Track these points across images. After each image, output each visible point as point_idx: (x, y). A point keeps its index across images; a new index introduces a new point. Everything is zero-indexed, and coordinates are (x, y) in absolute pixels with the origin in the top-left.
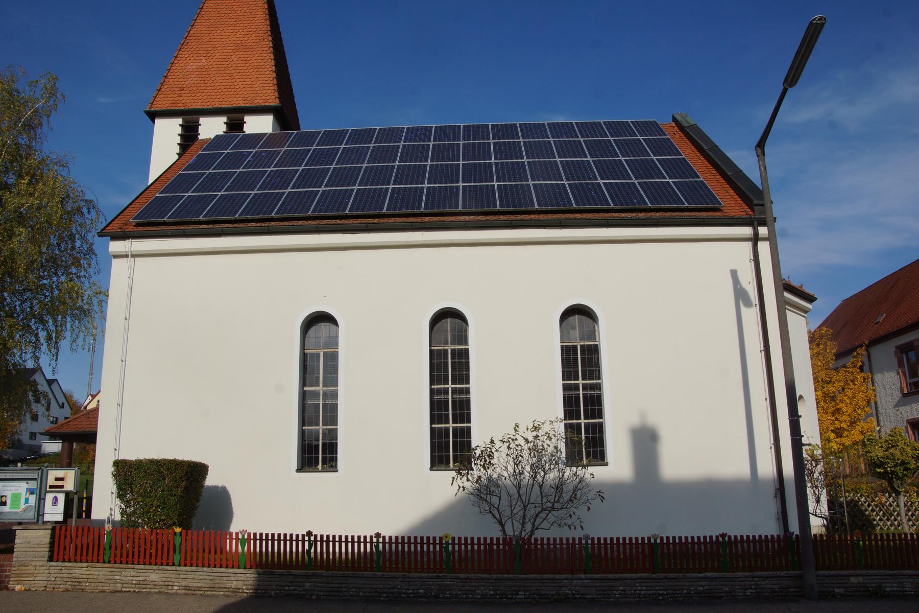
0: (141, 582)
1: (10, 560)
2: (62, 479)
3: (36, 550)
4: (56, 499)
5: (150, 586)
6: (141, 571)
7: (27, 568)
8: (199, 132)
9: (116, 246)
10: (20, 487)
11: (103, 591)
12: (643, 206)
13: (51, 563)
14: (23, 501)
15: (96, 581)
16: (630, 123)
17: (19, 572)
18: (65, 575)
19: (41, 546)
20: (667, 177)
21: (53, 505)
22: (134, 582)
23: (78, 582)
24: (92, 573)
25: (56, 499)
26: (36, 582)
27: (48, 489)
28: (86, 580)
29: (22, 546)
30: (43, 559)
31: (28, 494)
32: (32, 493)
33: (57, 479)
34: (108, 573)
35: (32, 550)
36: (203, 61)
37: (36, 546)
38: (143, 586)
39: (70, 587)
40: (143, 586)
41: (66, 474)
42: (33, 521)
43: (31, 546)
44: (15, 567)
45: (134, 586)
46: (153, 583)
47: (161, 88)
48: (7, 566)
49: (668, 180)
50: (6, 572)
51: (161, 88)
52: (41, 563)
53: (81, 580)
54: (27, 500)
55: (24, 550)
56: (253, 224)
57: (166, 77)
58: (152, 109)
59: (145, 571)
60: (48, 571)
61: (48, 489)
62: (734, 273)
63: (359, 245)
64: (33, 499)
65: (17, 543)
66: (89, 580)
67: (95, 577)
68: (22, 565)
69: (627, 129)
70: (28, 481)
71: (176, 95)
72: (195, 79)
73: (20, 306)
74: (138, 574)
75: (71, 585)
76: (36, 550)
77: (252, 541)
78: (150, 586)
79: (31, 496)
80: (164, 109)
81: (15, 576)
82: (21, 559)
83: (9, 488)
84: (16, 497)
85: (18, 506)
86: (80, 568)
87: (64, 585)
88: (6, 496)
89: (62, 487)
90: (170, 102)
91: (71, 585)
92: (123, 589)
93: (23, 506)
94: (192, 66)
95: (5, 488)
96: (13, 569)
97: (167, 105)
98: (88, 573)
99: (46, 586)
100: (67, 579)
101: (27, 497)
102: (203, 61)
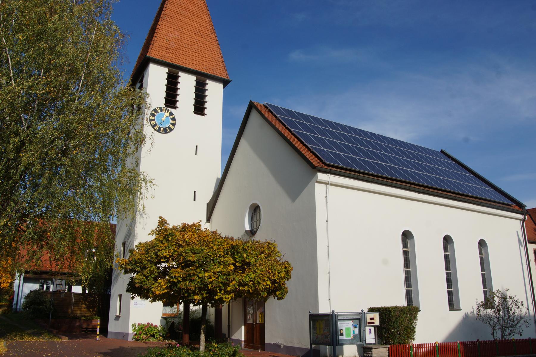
4: (370, 330)
10: (349, 324)
25: (370, 330)
27: (368, 325)
32: (356, 327)
33: (371, 319)
36: (177, 35)
41: (374, 316)
54: (354, 331)
58: (150, 56)
62: (517, 232)
63: (418, 199)
70: (353, 320)
73: (42, 175)
83: (345, 325)
84: (348, 330)
85: (349, 336)
89: (373, 323)
93: (352, 335)
101: (354, 330)
102: (177, 35)
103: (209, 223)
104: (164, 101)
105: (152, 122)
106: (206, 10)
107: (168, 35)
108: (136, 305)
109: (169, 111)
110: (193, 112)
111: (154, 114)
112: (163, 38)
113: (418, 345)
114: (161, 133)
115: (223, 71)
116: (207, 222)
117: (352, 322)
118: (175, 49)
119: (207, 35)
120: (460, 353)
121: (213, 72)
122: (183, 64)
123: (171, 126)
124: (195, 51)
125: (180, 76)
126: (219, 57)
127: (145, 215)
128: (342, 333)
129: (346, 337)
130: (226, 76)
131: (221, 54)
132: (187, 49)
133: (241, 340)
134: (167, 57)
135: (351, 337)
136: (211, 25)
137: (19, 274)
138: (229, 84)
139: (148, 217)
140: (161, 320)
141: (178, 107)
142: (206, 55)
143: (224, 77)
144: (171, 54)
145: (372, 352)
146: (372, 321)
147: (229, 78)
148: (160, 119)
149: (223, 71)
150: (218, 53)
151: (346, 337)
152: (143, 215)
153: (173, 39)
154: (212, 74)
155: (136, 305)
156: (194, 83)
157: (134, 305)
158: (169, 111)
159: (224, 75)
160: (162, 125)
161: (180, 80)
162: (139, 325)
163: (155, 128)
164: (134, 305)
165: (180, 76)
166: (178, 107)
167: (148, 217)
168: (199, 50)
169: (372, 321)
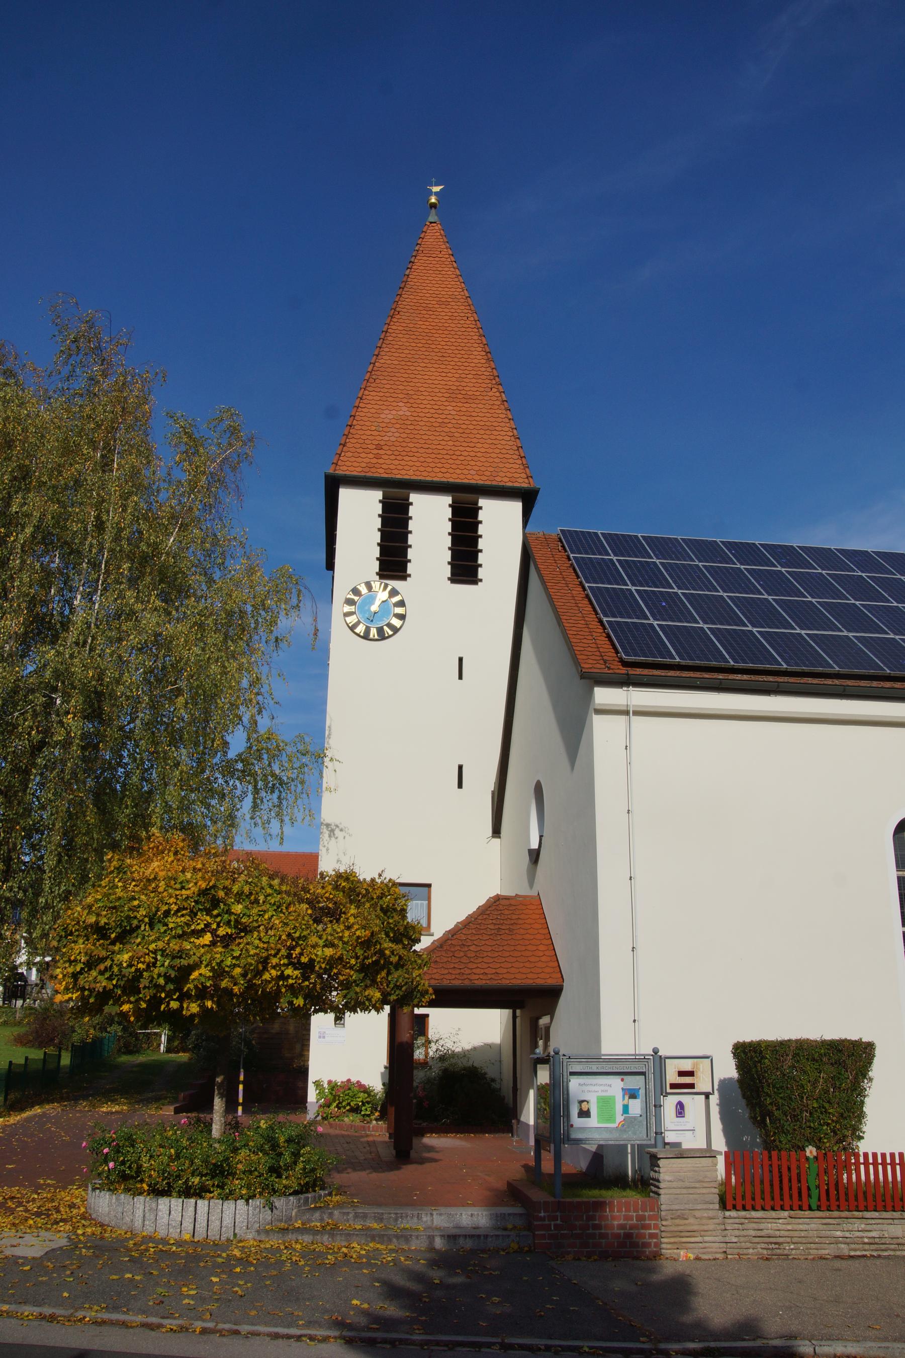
0: (877, 1240)
1: (656, 1206)
2: (691, 1074)
3: (698, 1191)
5: (892, 1247)
6: (873, 1221)
7: (686, 1222)
8: (410, 515)
9: (604, 695)
10: (610, 1086)
11: (822, 1258)
12: (723, 664)
13: (727, 1213)
14: (619, 1108)
15: (804, 1240)
16: (641, 538)
17: (676, 1229)
18: (753, 1233)
19: (705, 1185)
20: (650, 618)
21: (677, 1117)
22: (866, 1240)
23: (775, 1243)
24: (796, 1227)
26: (707, 1245)
27: (669, 1090)
28: (788, 1240)
29: (675, 1184)
30: (711, 1206)
31: (627, 1097)
33: (681, 1074)
34: (821, 1227)
35: (691, 1191)
36: (404, 411)
37: (697, 1185)
38: (883, 1247)
39: (765, 1252)
40: (883, 1247)
41: (694, 1065)
42: (649, 1142)
43: (687, 1184)
44: (666, 1220)
45: (867, 1247)
46: (895, 1241)
47: (346, 443)
48: (651, 1218)
49: (651, 621)
50: (651, 1229)
51: (346, 443)
52: (711, 1214)
53: (781, 1240)
54: (626, 1108)
55: (678, 1191)
56: (810, 680)
57: (351, 426)
58: (337, 472)
59: (880, 1221)
60: (723, 1227)
61: (669, 1090)
64: (636, 1107)
65: (665, 1181)
66: (795, 1240)
67: (803, 1234)
68: (679, 1217)
69: (595, 544)
70: (625, 1077)
71: (371, 456)
72: (397, 435)
74: (869, 1227)
75: (767, 1249)
76: (698, 1191)
77: (862, 1167)
78: (892, 1247)
79: (631, 1100)
80: (355, 473)
81: (669, 1235)
82: (676, 1207)
84: (606, 1103)
85: (611, 1119)
86: (774, 1221)
87: (753, 1249)
88: (588, 1102)
89: (692, 1086)
90: (364, 465)
91: (767, 1249)
92: (852, 1253)
93: (619, 1118)
94: (388, 416)
95: (584, 1088)
96: (664, 1223)
97: (360, 469)
98: (789, 1227)
99: (725, 1252)
100: (757, 1240)
101: (626, 1102)
102: (404, 411)
103: (500, 837)
104: (376, 566)
105: (349, 619)
106: (476, 337)
107: (382, 416)
108: (324, 1037)
109: (389, 588)
110: (449, 579)
111: (353, 600)
112: (371, 424)
113: (875, 1155)
114: (371, 640)
115: (518, 471)
116: (493, 837)
117: (622, 1080)
118: (398, 444)
119: (478, 393)
120: (809, 1189)
121: (492, 478)
122: (417, 473)
123: (396, 622)
124: (447, 438)
125: (481, 508)
126: (509, 438)
127: (341, 830)
128: (585, 1109)
129: (598, 1122)
130: (526, 481)
131: (515, 431)
132: (426, 437)
133: (528, 1125)
134: (376, 466)
135: (618, 1121)
136: (489, 369)
137: (173, 976)
138: (538, 497)
139: (347, 836)
140: (382, 1074)
141: (481, 580)
142: (474, 440)
143: (522, 483)
144: (387, 457)
145: (659, 1166)
146: (687, 1080)
147: (533, 484)
148: (366, 608)
149: (518, 471)
150: (507, 429)
151: (598, 1122)
152: (337, 832)
153: (392, 421)
154: (489, 483)
155: (324, 1037)
156: (449, 513)
157: (320, 1037)
158: (389, 588)
159: (520, 480)
160: (372, 621)
161: (481, 516)
162: (330, 1082)
163: (357, 630)
164: (320, 1037)
165: (481, 508)
166: (481, 580)
167: (347, 836)
168: (456, 435)
169: (687, 1080)
